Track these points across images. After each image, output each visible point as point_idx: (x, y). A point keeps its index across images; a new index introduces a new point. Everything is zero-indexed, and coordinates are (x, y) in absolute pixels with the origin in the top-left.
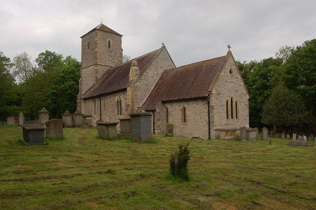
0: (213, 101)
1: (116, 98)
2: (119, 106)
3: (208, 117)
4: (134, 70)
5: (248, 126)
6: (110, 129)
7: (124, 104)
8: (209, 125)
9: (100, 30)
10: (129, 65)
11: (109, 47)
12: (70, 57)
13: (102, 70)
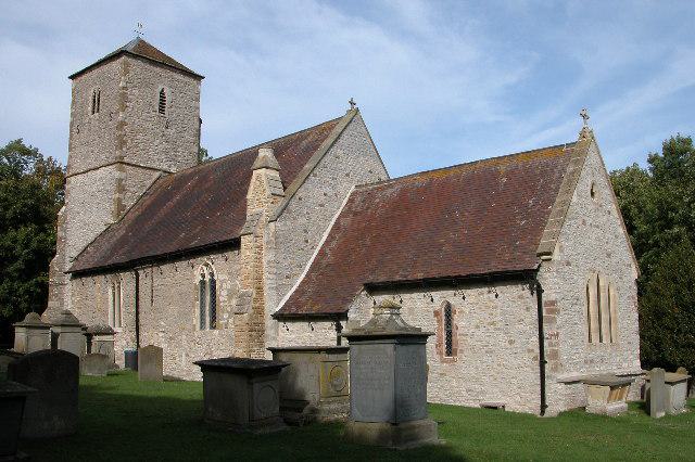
0: (547, 278)
1: (198, 270)
2: (208, 298)
3: (536, 339)
4: (262, 187)
5: (635, 365)
6: (257, 386)
7: (224, 293)
8: (542, 363)
9: (135, 56)
10: (240, 166)
11: (162, 110)
12: (19, 141)
13: (139, 184)
